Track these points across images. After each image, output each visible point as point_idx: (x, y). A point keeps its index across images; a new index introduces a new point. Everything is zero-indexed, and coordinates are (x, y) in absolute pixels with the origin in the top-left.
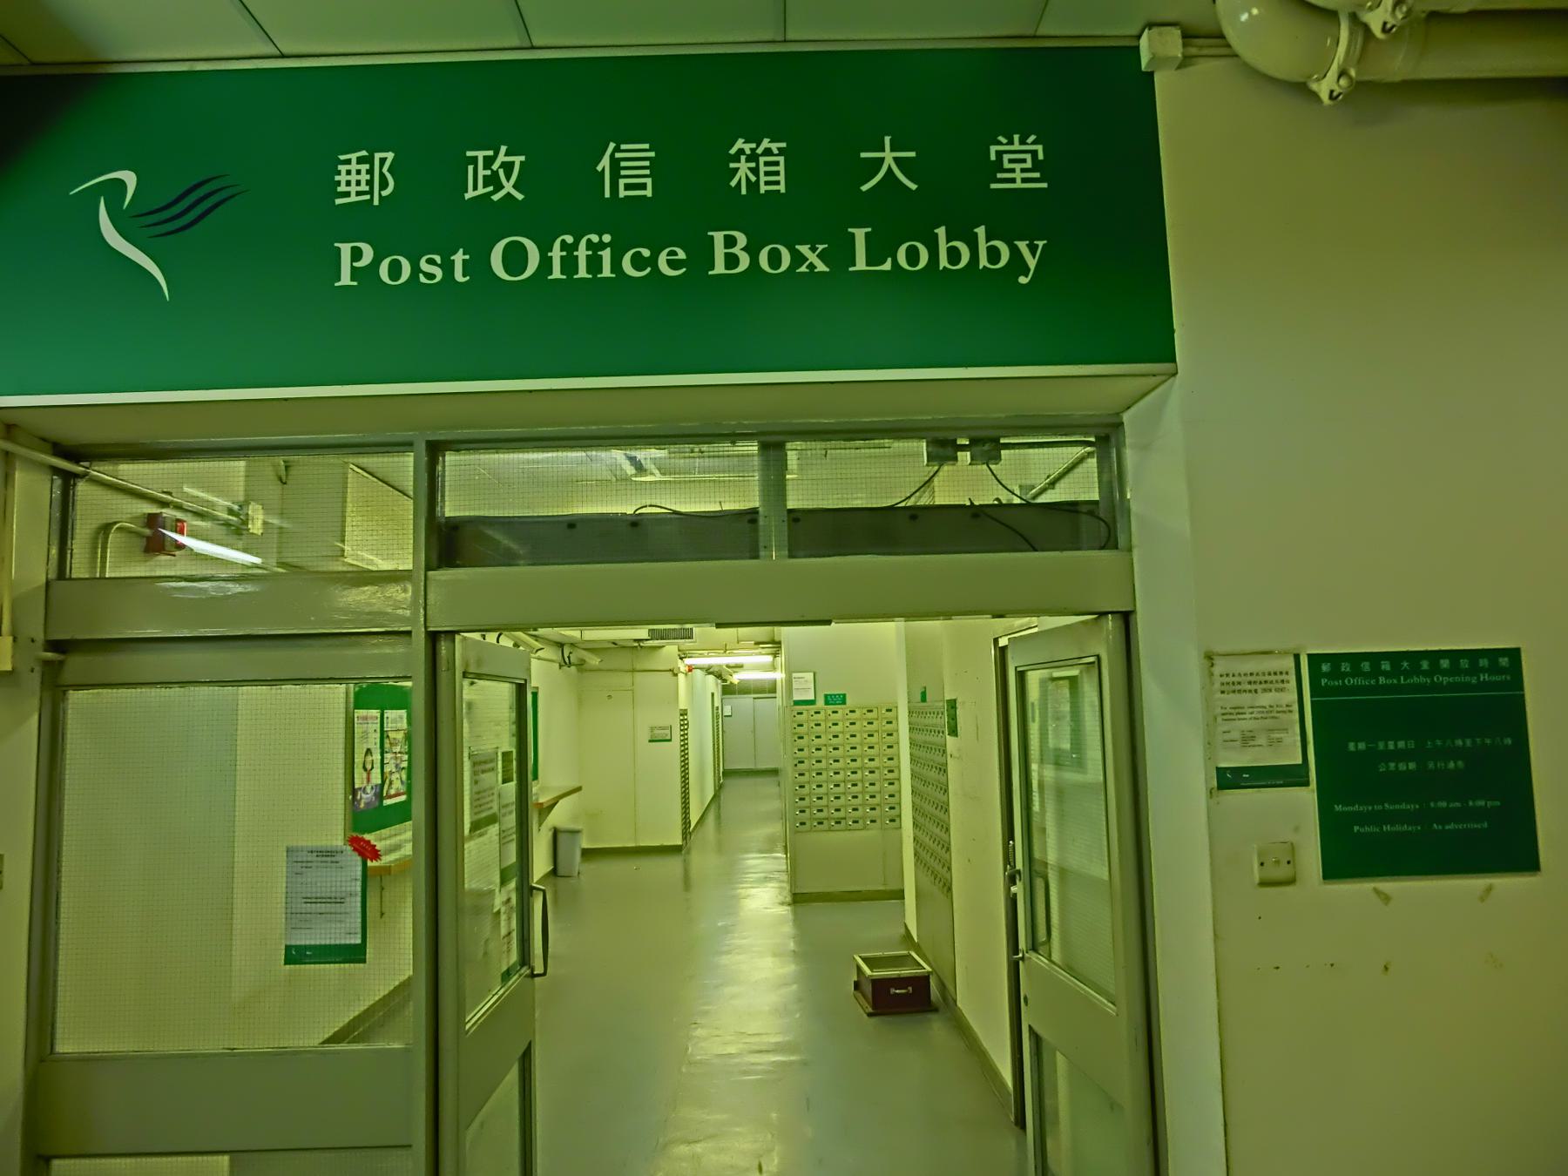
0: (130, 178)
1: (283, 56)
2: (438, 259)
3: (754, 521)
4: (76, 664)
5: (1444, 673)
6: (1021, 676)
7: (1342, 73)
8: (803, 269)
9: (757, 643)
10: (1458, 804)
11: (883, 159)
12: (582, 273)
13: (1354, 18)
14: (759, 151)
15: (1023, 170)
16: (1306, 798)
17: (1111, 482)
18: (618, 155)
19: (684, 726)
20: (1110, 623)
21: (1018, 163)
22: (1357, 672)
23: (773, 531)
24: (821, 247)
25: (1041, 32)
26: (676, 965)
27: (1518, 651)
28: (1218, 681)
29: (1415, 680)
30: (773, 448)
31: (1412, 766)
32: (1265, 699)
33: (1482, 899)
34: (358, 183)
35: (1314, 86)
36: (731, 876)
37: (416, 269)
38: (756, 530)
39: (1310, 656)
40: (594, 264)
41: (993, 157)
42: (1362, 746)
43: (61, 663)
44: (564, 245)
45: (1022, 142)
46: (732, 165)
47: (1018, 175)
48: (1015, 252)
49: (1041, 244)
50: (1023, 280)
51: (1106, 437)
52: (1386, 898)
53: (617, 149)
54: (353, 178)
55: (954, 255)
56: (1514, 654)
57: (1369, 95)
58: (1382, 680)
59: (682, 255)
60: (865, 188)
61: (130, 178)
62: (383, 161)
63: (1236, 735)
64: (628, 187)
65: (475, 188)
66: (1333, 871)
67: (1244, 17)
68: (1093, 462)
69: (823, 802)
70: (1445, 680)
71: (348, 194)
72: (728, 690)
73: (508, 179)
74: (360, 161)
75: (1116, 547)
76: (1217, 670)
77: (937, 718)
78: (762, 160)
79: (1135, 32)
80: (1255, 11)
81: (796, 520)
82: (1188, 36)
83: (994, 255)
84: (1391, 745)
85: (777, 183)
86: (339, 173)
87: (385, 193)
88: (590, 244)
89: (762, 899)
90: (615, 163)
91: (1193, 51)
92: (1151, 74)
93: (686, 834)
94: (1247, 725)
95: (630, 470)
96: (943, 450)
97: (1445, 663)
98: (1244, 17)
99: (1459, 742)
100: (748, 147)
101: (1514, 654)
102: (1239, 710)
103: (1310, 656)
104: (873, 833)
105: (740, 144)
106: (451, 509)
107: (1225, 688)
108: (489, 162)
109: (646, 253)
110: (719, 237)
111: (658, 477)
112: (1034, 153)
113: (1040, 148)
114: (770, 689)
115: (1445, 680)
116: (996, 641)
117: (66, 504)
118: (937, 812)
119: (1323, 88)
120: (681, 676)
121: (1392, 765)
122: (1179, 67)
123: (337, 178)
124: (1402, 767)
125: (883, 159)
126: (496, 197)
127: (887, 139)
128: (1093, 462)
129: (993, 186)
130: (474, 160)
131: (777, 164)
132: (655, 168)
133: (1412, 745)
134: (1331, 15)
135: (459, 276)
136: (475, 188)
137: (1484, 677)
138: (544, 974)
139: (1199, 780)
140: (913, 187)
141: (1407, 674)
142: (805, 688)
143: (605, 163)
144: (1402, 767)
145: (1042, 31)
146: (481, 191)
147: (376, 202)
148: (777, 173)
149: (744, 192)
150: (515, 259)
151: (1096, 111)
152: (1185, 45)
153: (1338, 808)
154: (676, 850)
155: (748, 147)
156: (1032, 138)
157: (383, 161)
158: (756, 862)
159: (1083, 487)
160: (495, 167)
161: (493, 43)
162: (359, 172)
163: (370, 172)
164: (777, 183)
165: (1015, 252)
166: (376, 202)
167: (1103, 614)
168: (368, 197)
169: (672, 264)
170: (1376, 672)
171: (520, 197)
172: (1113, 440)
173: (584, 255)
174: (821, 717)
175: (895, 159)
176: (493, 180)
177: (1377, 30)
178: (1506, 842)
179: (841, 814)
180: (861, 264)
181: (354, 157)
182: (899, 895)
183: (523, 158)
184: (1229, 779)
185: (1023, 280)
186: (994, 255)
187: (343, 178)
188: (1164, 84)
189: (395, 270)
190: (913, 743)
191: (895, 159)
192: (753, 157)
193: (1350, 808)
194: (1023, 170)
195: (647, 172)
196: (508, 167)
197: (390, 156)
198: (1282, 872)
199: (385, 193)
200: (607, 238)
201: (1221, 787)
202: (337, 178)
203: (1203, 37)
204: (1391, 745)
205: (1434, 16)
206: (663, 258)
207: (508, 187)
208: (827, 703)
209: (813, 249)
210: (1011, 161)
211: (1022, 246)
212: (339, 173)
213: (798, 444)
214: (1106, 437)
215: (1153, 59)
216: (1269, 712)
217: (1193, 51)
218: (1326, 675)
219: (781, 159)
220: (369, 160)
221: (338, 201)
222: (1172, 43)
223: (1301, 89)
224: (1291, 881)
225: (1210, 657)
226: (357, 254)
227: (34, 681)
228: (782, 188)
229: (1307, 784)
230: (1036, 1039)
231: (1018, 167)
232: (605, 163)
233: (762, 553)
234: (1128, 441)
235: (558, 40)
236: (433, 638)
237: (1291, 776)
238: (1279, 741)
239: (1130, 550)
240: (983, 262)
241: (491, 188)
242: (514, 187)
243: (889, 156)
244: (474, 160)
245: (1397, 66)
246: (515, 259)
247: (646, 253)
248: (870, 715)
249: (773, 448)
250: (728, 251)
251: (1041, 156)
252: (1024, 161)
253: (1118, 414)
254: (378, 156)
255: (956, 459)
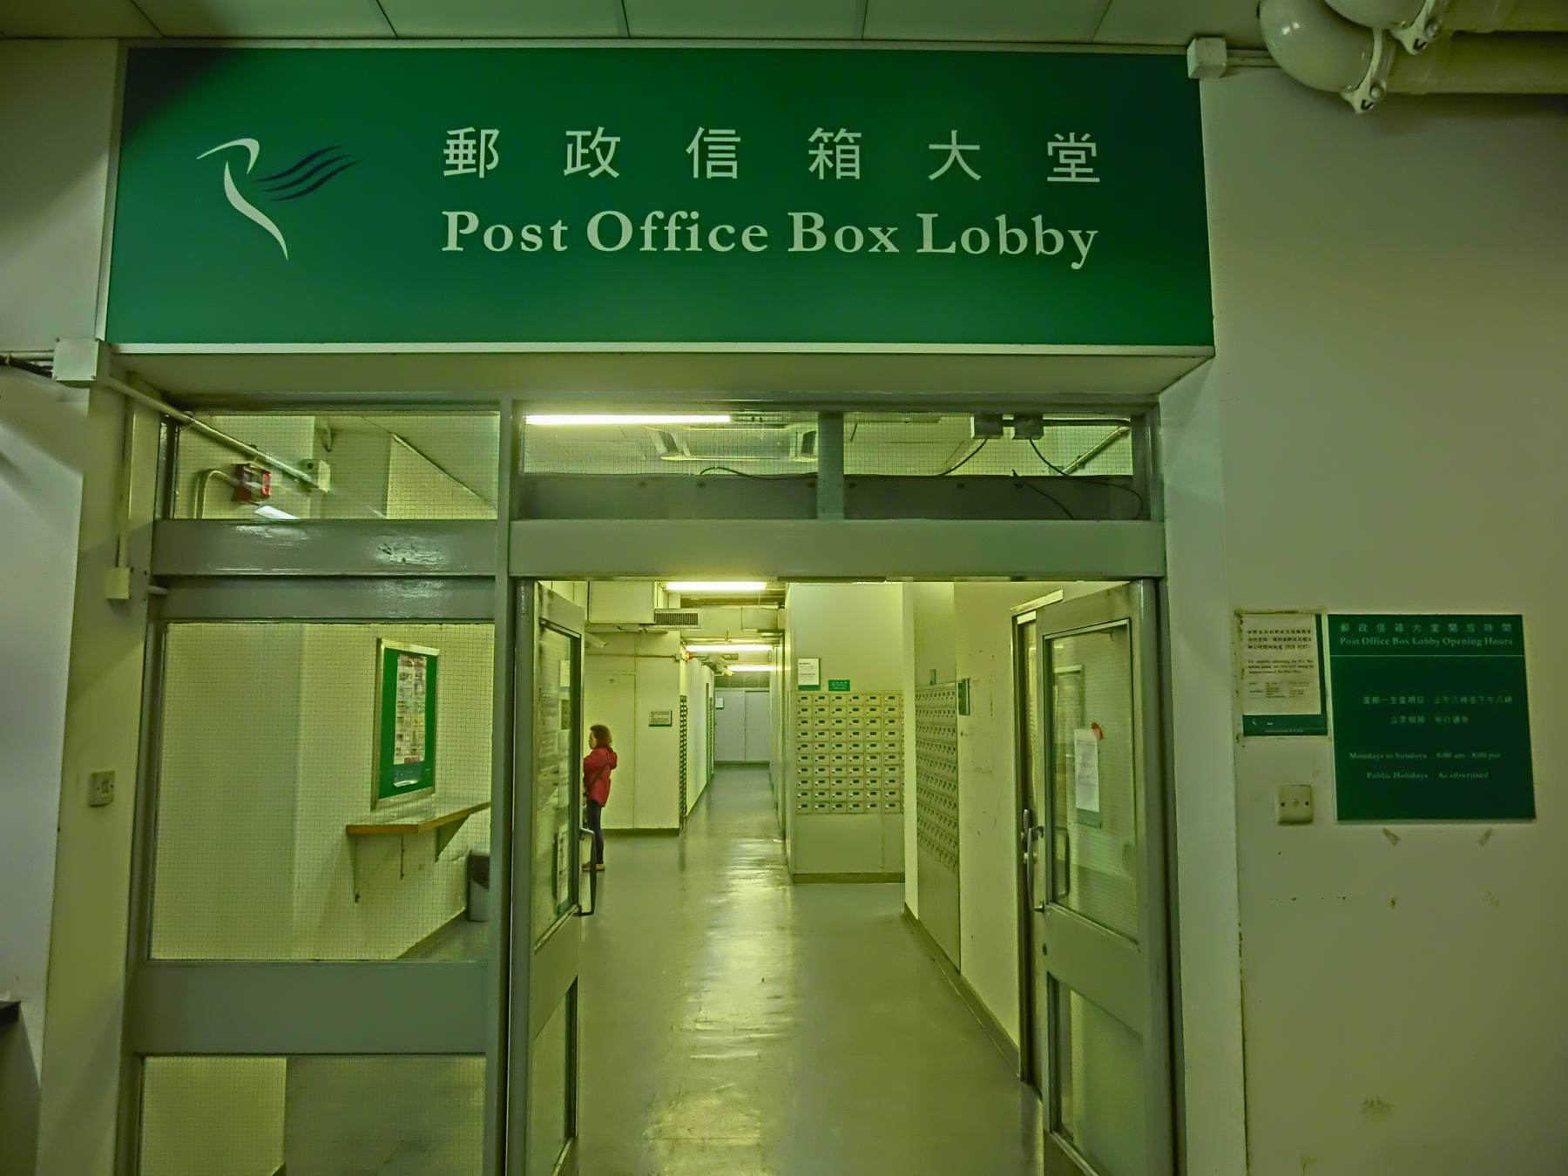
0: (253, 146)
1: (397, 38)
2: (538, 229)
3: (813, 485)
4: (179, 598)
5: (1453, 636)
6: (1048, 645)
7: (1374, 85)
8: (875, 249)
9: (760, 631)
10: (1462, 756)
11: (949, 151)
12: (672, 246)
13: (1387, 34)
14: (837, 140)
15: (1078, 166)
16: (1324, 747)
17: (1144, 459)
18: (706, 139)
19: (684, 711)
20: (1140, 589)
21: (1073, 159)
22: (1372, 632)
23: (830, 493)
24: (892, 230)
25: (1097, 39)
26: (684, 937)
27: (1519, 618)
28: (1246, 636)
29: (1427, 642)
30: (832, 418)
31: (1421, 719)
32: (1288, 655)
33: (1482, 842)
34: (465, 157)
35: (1347, 96)
36: (719, 861)
37: (518, 238)
38: (814, 495)
39: (1330, 616)
40: (683, 238)
41: (1050, 153)
42: (1376, 700)
43: (164, 597)
44: (655, 220)
45: (1078, 139)
46: (811, 152)
47: (1073, 170)
48: (1069, 240)
49: (1092, 233)
50: (1075, 266)
51: (1140, 415)
52: (1395, 839)
53: (706, 134)
54: (461, 152)
55: (1013, 241)
56: (1516, 621)
57: (1396, 106)
58: (1395, 640)
59: (763, 233)
60: (932, 177)
61: (253, 146)
62: (488, 137)
63: (1262, 686)
64: (715, 169)
65: (574, 165)
66: (1347, 812)
67: (1286, 31)
68: (1127, 442)
69: (826, 786)
70: (1453, 642)
71: (455, 167)
72: (721, 682)
74: (467, 136)
75: (1148, 518)
76: (1245, 627)
77: (943, 699)
78: (839, 148)
79: (1183, 41)
80: (1296, 26)
81: (852, 485)
82: (1231, 47)
83: (1049, 242)
84: (1402, 700)
85: (853, 170)
86: (448, 147)
87: (490, 167)
88: (679, 221)
89: (752, 888)
90: (703, 147)
91: (1236, 61)
92: (1197, 81)
93: (683, 819)
94: (1272, 677)
95: (661, 448)
96: (990, 425)
97: (1453, 627)
98: (1286, 31)
99: (1465, 699)
100: (826, 136)
101: (1516, 621)
102: (1264, 664)
103: (1330, 616)
104: (873, 817)
105: (818, 132)
106: (529, 467)
107: (1253, 643)
108: (586, 142)
109: (731, 230)
110: (798, 217)
111: (688, 457)
112: (1088, 150)
113: (1093, 146)
114: (763, 682)
115: (1453, 642)
116: (1014, 618)
117: (172, 447)
118: (945, 791)
119: (1356, 98)
120: (682, 663)
121: (1403, 718)
122: (1225, 74)
124: (1412, 719)
125: (949, 151)
126: (593, 174)
127: (954, 133)
128: (1128, 441)
129: (1050, 179)
131: (852, 152)
132: (741, 153)
133: (1421, 700)
134: (1365, 31)
135: (558, 246)
136: (574, 165)
137: (1489, 641)
138: (592, 913)
139: (1226, 728)
140: (977, 177)
141: (1419, 636)
142: (810, 672)
143: (694, 146)
144: (1412, 719)
145: (1098, 38)
146: (579, 167)
147: (482, 175)
148: (852, 161)
149: (822, 176)
150: (610, 231)
151: (1143, 116)
152: (1229, 56)
153: (1353, 756)
154: (673, 833)
155: (826, 136)
156: (1087, 136)
157: (488, 137)
158: (756, 847)
159: (1118, 463)
160: (592, 146)
161: (592, 29)
162: (466, 147)
163: (477, 147)
164: (853, 170)
165: (1069, 240)
166: (482, 175)
167: (1134, 579)
169: (755, 241)
170: (1390, 633)
171: (615, 174)
172: (1148, 419)
173: (673, 229)
174: (826, 701)
175: (961, 152)
176: (590, 159)
177: (1409, 47)
178: (1505, 792)
179: (843, 797)
180: (928, 247)
181: (461, 132)
182: (900, 878)
184: (1255, 726)
185: (1075, 266)
186: (1049, 242)
187: (451, 152)
188: (1209, 94)
189: (498, 238)
190: (919, 726)
191: (961, 152)
192: (831, 145)
193: (1363, 756)
194: (1078, 166)
196: (604, 147)
197: (495, 133)
198: (1301, 812)
199: (490, 167)
200: (695, 215)
201: (1246, 733)
203: (1248, 49)
204: (1402, 700)
205: (1460, 35)
206: (746, 234)
207: (605, 165)
208: (831, 689)
209: (884, 232)
210: (1067, 157)
211: (1076, 234)
212: (448, 147)
213: (857, 415)
214: (1140, 415)
215: (1202, 68)
216: (1291, 667)
217: (1236, 61)
218: (1344, 634)
219: (856, 148)
221: (447, 173)
222: (1217, 53)
223: (1335, 99)
224: (1308, 821)
225: (1239, 615)
226: (463, 222)
227: (141, 609)
228: (857, 175)
229: (1325, 733)
230: (1053, 984)
231: (1073, 162)
232: (694, 146)
233: (820, 514)
234: (1163, 419)
235: (657, 27)
236: (514, 582)
237: (1312, 726)
238: (1301, 693)
239: (1162, 520)
240: (1040, 248)
243: (955, 149)
244: (573, 140)
245: (1425, 80)
246: (610, 231)
247: (731, 230)
248: (873, 702)
249: (832, 418)
250: (807, 230)
251: (1094, 154)
252: (1079, 157)
253: (1154, 395)
254: (484, 133)
255: (1001, 433)
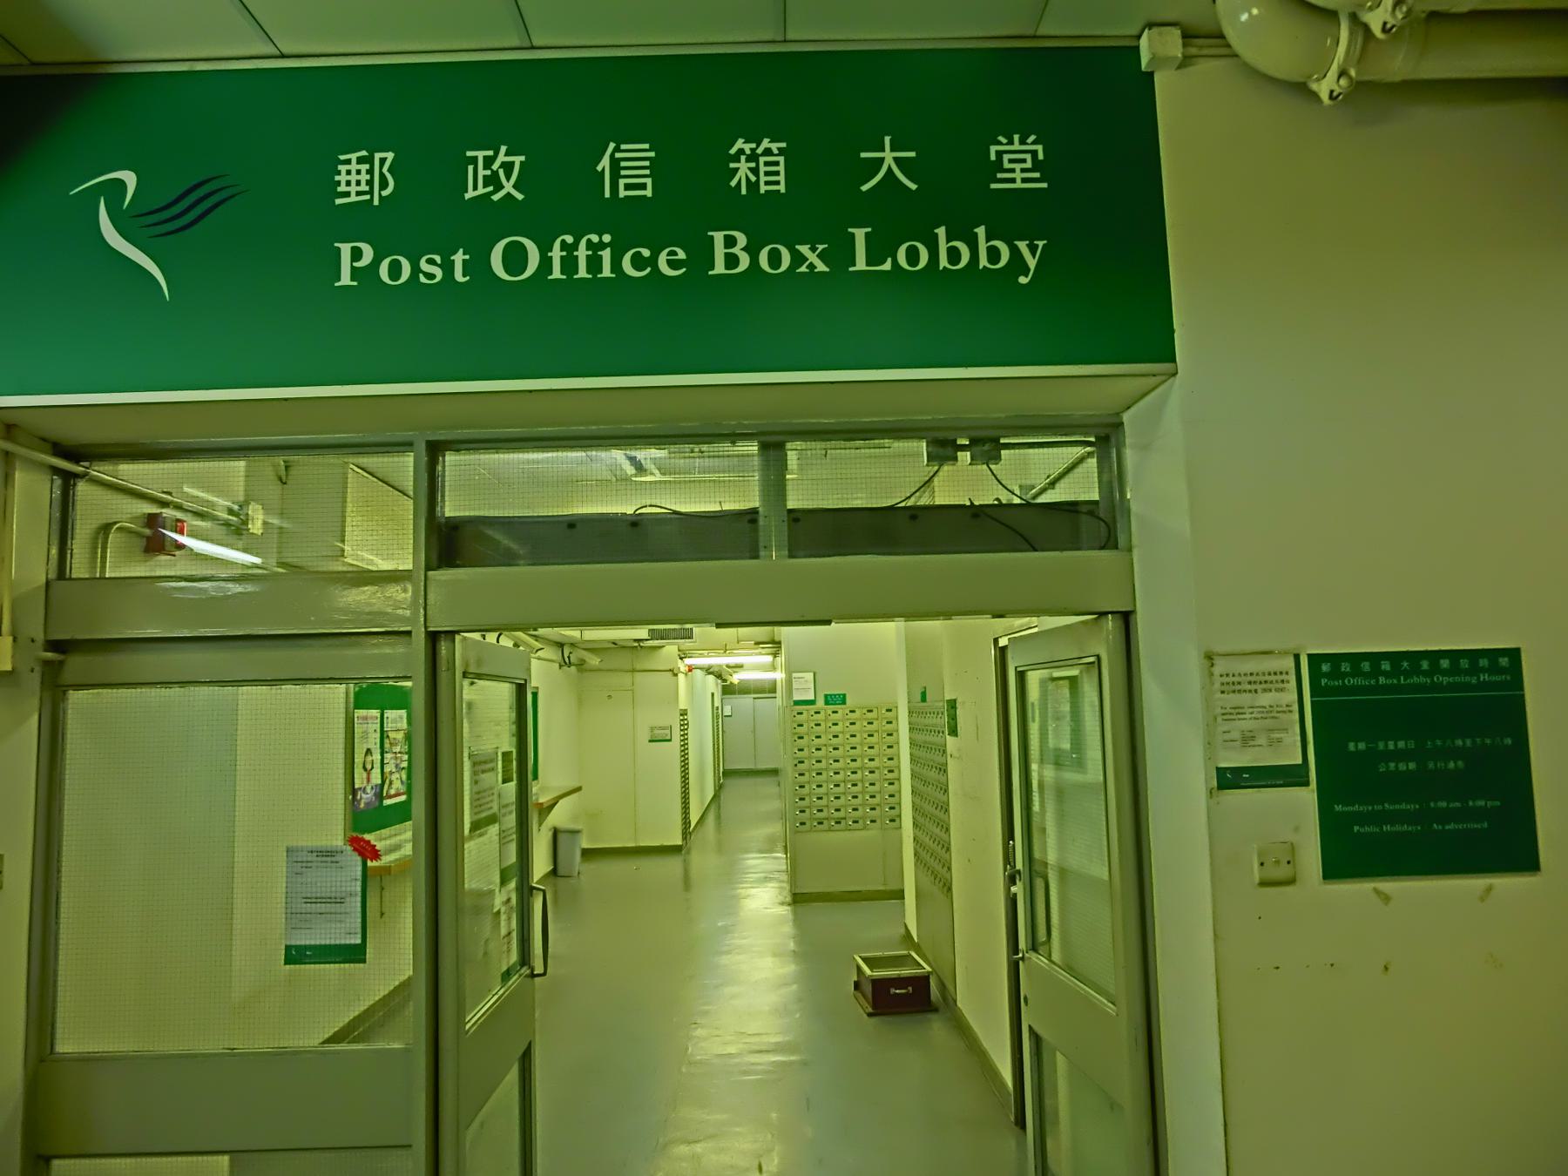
0: (130, 178)
1: (283, 56)
2: (438, 259)
3: (754, 521)
4: (76, 664)
5: (1444, 673)
6: (1021, 676)
7: (1342, 73)
8: (803, 269)
9: (757, 643)
10: (1458, 804)
11: (883, 159)
12: (582, 273)
13: (1354, 18)
14: (759, 151)
15: (1023, 170)
16: (1306, 798)
17: (1111, 482)
18: (618, 155)
19: (684, 726)
20: (1110, 623)
21: (1018, 163)
22: (1357, 672)
23: (773, 531)
24: (821, 247)
25: (1041, 32)
26: (676, 965)
27: (1518, 651)
28: (1218, 681)
29: (1415, 680)
30: (773, 448)
31: (1412, 766)
32: (1265, 699)
33: (1482, 899)
34: (358, 183)
35: (1314, 86)
36: (731, 876)
37: (416, 269)
38: (756, 530)
39: (1310, 656)
40: (594, 264)
41: (993, 157)
42: (1362, 746)
43: (61, 663)
44: (564, 245)
45: (1022, 142)
46: (732, 165)
47: (1018, 175)
48: (1015, 252)
49: (1041, 244)
50: (1023, 280)
51: (1106, 437)
52: (1386, 898)
53: (617, 149)
54: (353, 178)
55: (954, 255)
56: (1514, 654)
57: (1369, 95)
58: (1382, 680)
59: (682, 255)
60: (865, 188)
61: (130, 178)
62: (383, 161)
63: (1236, 735)
64: (628, 187)
65: (475, 188)
66: (1333, 871)
67: (1244, 17)
68: (1093, 462)
69: (823, 802)
70: (1445, 680)
71: (348, 194)
72: (728, 690)
73: (508, 179)
74: (360, 161)
75: (1116, 547)
76: (1217, 670)
77: (937, 718)
78: (762, 160)
79: (1135, 32)
80: (1255, 11)
81: (796, 520)
82: (1188, 36)
83: (994, 255)
84: (1391, 745)
85: (777, 183)
86: (339, 173)
87: (385, 193)
88: (590, 244)
89: (762, 899)
90: (615, 163)
91: (1193, 51)
92: (1151, 74)
93: (686, 834)
94: (1247, 725)
95: (630, 470)
96: (943, 450)
97: (1445, 663)
98: (1244, 17)
99: (1459, 742)
100: (748, 147)
101: (1514, 654)
102: (1239, 710)
103: (1310, 656)
104: (873, 833)
105: (740, 144)
106: (451, 509)
107: (1225, 688)
108: (489, 162)
109: (646, 253)
110: (719, 237)
111: (658, 477)
112: (1034, 153)
113: (1040, 148)
114: (770, 689)
115: (1445, 680)
116: (996, 641)
117: (66, 504)
118: (937, 812)
119: (1323, 88)
120: (681, 676)
121: (1392, 765)
122: (1179, 67)
123: (337, 178)
124: (1402, 767)
125: (883, 159)
126: (496, 197)
127: (887, 139)
128: (1093, 462)
129: (993, 186)
130: (474, 160)
131: (777, 164)
132: (655, 168)
133: (1412, 745)
134: (1331, 15)
135: (459, 276)
136: (475, 188)
137: (1484, 677)
138: (544, 974)
139: (1199, 780)
140: (913, 187)
141: (1407, 674)
142: (805, 688)
143: (605, 163)
144: (1402, 767)
145: (1042, 31)
146: (481, 191)
147: (376, 202)
148: (777, 173)
149: (744, 192)
150: (515, 259)
151: (1096, 111)
152: (1185, 45)
153: (1338, 808)
154: (676, 850)
155: (748, 147)
156: (1032, 138)
157: (383, 161)
158: (756, 862)
159: (1083, 487)
160: (495, 167)
161: (493, 43)
162: (359, 172)
163: (370, 172)
164: (777, 183)
165: (1015, 252)
166: (376, 202)
167: (1103, 614)
168: (368, 197)
169: (672, 264)
170: (1376, 672)
171: (520, 197)
172: (1113, 440)
173: (584, 255)
174: (821, 717)
175: (895, 159)
176: (493, 180)
177: (1377, 30)
178: (1506, 842)
179: (841, 814)
180: (861, 264)
181: (354, 157)
182: (899, 895)
183: (523, 158)
184: (1229, 779)
185: (1023, 280)
186: (994, 255)
187: (343, 178)
188: (1164, 84)
189: (395, 270)
190: (913, 743)
191: (895, 159)
192: (753, 157)
193: (1350, 808)
194: (1023, 170)
195: (647, 172)
196: (508, 167)
197: (390, 156)
198: (1282, 872)
199: (385, 193)
200: (607, 238)
201: (1221, 787)
202: (337, 178)
203: (1203, 37)
204: (1391, 745)
205: (1434, 16)
206: (663, 258)
207: (508, 187)
208: (827, 703)
209: (813, 249)
210: (1011, 161)
211: (1022, 246)
212: (339, 173)
213: (798, 444)
214: (1106, 437)
215: (1153, 59)
216: (1269, 712)
217: (1193, 51)
218: (1326, 675)
219: (781, 159)
220: (369, 160)
221: (338, 201)
222: (1172, 43)
223: (1301, 89)
224: (1291, 881)
225: (1210, 657)
226: (357, 254)
227: (34, 681)
228: (782, 188)
229: (1307, 784)
230: (1036, 1039)
231: (1018, 167)
232: (605, 163)
233: (762, 553)
234: (1128, 441)
235: (558, 40)
236: (433, 638)
237: (1291, 776)
238: (1279, 741)
239: (1130, 550)
240: (983, 262)
241: (491, 188)
242: (514, 187)
243: (889, 156)
244: (474, 160)
245: (1397, 66)
246: (515, 259)
247: (646, 253)
248: (870, 715)
249: (773, 448)
250: (728, 251)
251: (1041, 156)
252: (1024, 161)
253: (1118, 414)
254: (378, 156)
255: (956, 459)
